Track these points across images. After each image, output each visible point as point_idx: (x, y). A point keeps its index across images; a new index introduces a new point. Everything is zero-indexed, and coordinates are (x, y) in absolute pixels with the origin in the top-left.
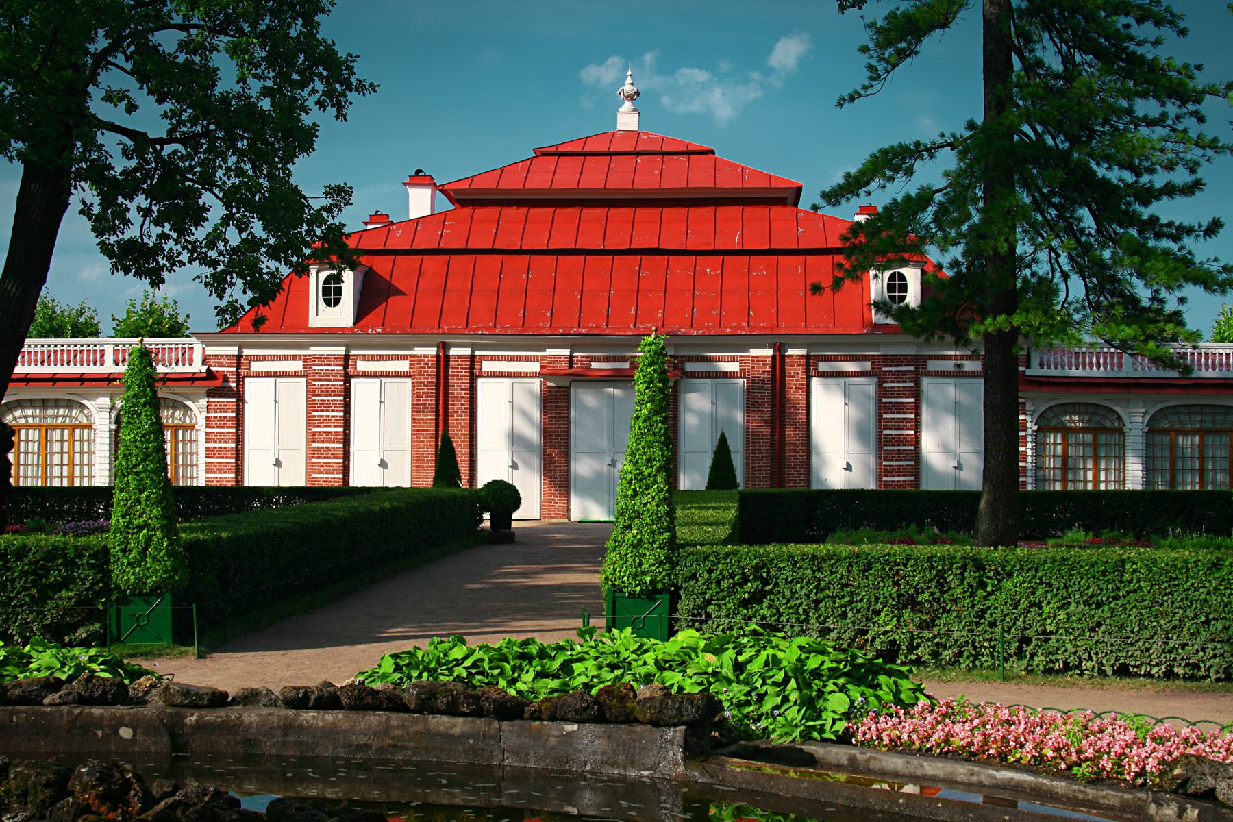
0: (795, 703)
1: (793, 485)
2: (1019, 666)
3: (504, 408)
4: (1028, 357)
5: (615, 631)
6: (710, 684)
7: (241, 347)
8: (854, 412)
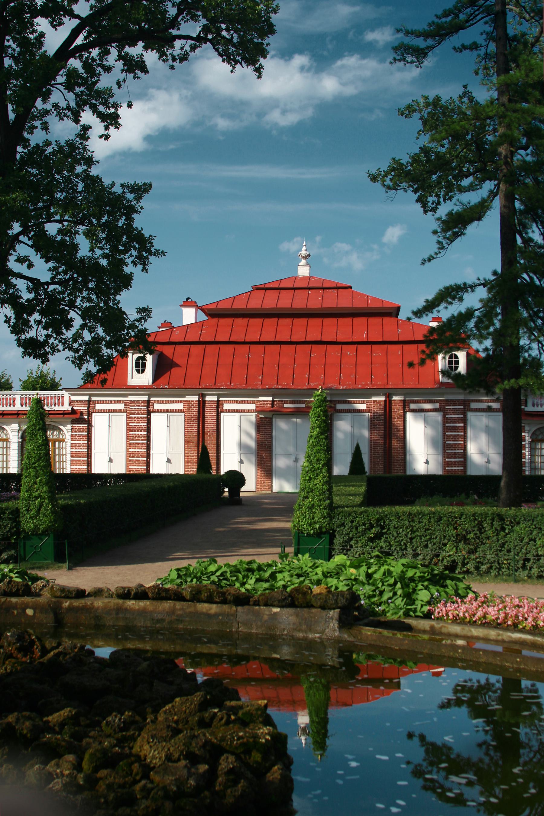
0: (400, 596)
1: (396, 472)
2: (523, 574)
3: (235, 429)
4: (526, 401)
5: (300, 556)
6: (353, 585)
7: (90, 396)
8: (430, 431)
